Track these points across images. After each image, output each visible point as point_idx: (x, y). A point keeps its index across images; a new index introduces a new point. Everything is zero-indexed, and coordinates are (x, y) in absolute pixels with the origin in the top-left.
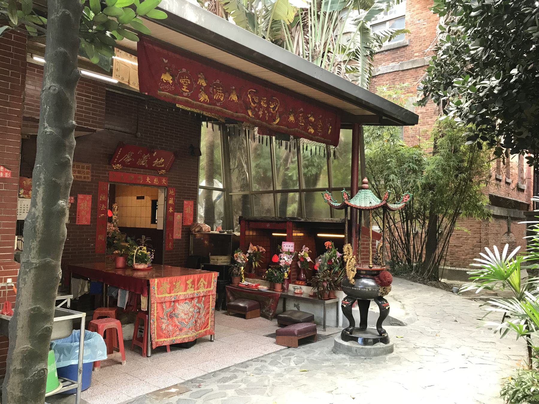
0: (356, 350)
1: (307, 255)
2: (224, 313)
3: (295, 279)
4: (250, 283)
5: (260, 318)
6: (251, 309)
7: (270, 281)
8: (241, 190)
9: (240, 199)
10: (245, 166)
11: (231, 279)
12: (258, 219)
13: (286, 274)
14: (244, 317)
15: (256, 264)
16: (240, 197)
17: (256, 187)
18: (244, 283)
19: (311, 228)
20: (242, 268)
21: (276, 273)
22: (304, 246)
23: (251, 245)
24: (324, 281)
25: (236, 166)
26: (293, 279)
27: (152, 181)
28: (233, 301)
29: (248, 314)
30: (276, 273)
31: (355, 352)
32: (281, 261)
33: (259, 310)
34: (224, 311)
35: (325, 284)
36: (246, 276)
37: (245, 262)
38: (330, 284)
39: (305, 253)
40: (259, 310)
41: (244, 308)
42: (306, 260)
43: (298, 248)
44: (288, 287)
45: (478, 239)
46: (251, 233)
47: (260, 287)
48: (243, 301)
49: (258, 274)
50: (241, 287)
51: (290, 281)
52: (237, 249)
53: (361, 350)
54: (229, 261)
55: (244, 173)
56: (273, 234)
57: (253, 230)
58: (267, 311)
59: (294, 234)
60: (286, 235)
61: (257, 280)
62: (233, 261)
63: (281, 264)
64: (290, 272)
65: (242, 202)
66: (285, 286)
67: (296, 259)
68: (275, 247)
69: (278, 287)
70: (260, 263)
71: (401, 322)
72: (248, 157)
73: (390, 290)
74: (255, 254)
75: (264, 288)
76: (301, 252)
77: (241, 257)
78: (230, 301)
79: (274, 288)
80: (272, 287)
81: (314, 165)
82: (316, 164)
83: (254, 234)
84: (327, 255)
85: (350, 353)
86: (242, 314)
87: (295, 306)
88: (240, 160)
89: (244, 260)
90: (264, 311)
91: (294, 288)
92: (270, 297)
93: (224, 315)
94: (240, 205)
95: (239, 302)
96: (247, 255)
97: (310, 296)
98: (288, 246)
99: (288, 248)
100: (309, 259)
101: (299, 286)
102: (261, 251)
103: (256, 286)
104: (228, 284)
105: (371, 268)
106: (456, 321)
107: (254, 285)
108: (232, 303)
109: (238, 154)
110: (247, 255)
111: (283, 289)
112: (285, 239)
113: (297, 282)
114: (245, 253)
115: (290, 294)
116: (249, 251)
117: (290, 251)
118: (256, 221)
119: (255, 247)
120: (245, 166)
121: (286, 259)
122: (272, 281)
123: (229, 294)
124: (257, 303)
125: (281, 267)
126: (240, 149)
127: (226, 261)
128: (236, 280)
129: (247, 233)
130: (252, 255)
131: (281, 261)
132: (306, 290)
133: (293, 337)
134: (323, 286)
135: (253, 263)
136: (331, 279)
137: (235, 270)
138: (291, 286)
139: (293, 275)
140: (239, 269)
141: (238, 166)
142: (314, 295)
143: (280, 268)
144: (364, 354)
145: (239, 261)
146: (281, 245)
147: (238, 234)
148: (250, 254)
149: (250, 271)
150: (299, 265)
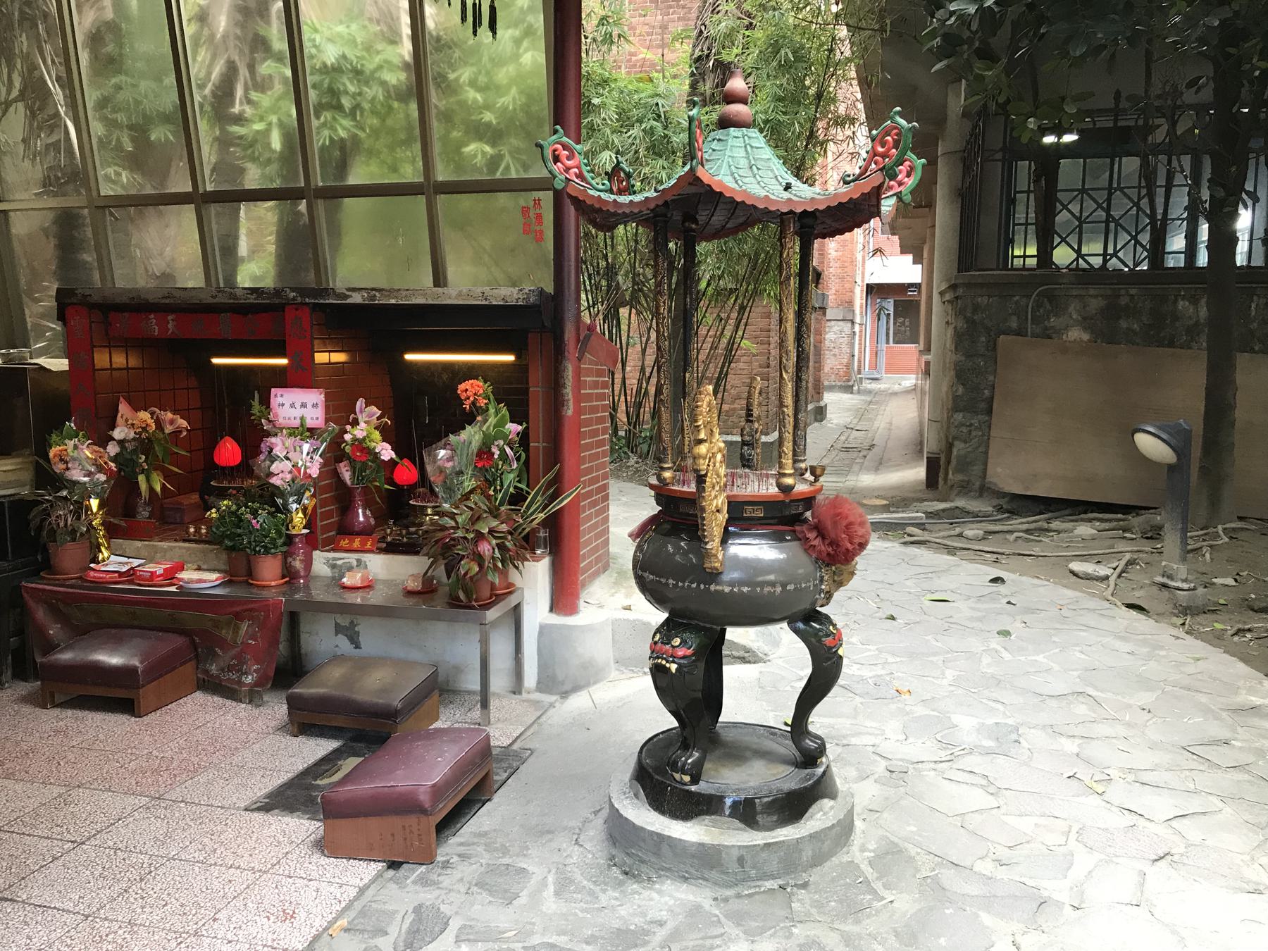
0: (741, 860)
1: (377, 435)
2: (25, 700)
3: (336, 528)
4: (136, 562)
5: (199, 696)
6: (159, 669)
7: (230, 549)
8: (47, 193)
9: (45, 231)
10: (58, 94)
11: (45, 549)
12: (151, 298)
13: (298, 518)
14: (128, 707)
15: (929, 881)
16: (47, 219)
17: (115, 179)
18: (112, 562)
19: (378, 330)
20: (94, 503)
21: (255, 513)
22: (360, 403)
23: (124, 408)
24: (480, 536)
25: (15, 93)
26: (326, 529)
27: (198, 530)
28: (69, 647)
29: (146, 694)
30: (255, 513)
31: (733, 867)
32: (275, 468)
33: (189, 668)
34: (24, 688)
35: (485, 548)
36: (113, 532)
37: (103, 478)
38: (501, 547)
39: (366, 426)
40: (189, 668)
41: (124, 674)
42: (376, 456)
43: (340, 411)
44: (308, 563)
45: (763, 359)
46: (119, 360)
47: (185, 575)
48: (115, 643)
49: (167, 520)
50: (98, 584)
51: (312, 542)
52: (59, 426)
53: (764, 855)
54: (27, 476)
55: (54, 123)
56: (215, 361)
57: (126, 344)
58: (230, 669)
59: (321, 358)
60: (284, 361)
61: (164, 544)
62: (47, 478)
63: (275, 481)
64: (315, 508)
65: (53, 242)
66: (298, 564)
67: (335, 453)
68: (235, 411)
69: (269, 569)
70: (168, 476)
71: (748, 651)
72: (67, 57)
73: (853, 574)
74: (145, 444)
75: (203, 578)
76: (355, 423)
77: (79, 459)
78: (50, 647)
79: (250, 573)
80: (240, 571)
81: (339, 107)
82: (346, 103)
83: (133, 362)
84: (471, 436)
85: (714, 874)
86: (118, 695)
87: (339, 629)
88: (33, 67)
89: (100, 469)
90: (213, 669)
91: (333, 567)
92: (238, 617)
93: (27, 709)
94: (48, 250)
95: (95, 649)
96: (113, 449)
97: (410, 593)
98: (297, 406)
99: (298, 412)
100: (386, 452)
101: (352, 558)
102: (169, 429)
103: (170, 576)
104: (35, 574)
105: (786, 489)
106: (892, 618)
107: (159, 570)
108: (66, 656)
109: (23, 42)
110: (113, 449)
111: (289, 575)
112: (282, 379)
113: (344, 543)
114: (102, 440)
115: (319, 594)
116: (118, 434)
117: (310, 423)
118: (139, 306)
119: (144, 415)
120: (58, 94)
121: (293, 460)
122: (237, 552)
123: (41, 614)
124: (178, 641)
125: (276, 491)
126: (28, 21)
127: (11, 477)
128: (68, 556)
129: (101, 359)
130: (130, 446)
131: (275, 468)
132: (384, 571)
133: (412, 820)
134: (479, 559)
135: (141, 478)
136: (504, 527)
137: (62, 515)
138: (321, 562)
139: (328, 515)
140: (80, 509)
141: (22, 92)
142: (427, 590)
143: (270, 496)
144: (774, 866)
145: (77, 475)
146: (266, 401)
147: (59, 364)
148: (121, 443)
149: (129, 512)
150: (347, 476)
